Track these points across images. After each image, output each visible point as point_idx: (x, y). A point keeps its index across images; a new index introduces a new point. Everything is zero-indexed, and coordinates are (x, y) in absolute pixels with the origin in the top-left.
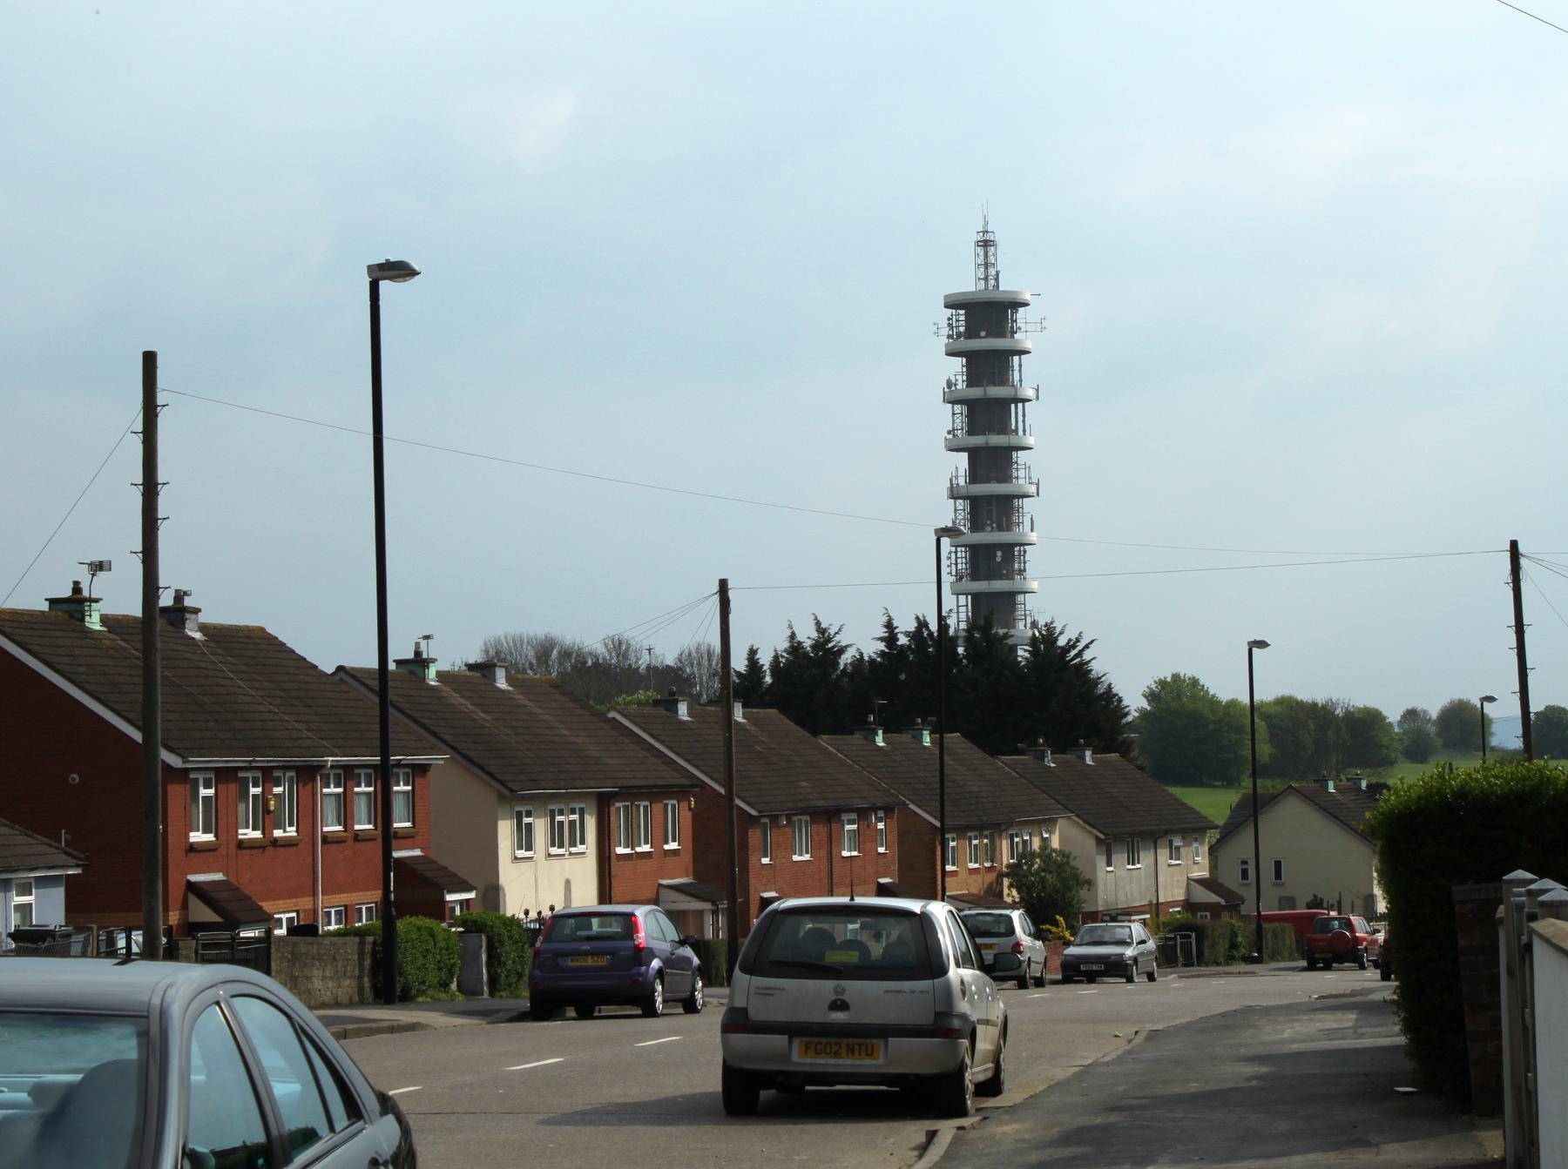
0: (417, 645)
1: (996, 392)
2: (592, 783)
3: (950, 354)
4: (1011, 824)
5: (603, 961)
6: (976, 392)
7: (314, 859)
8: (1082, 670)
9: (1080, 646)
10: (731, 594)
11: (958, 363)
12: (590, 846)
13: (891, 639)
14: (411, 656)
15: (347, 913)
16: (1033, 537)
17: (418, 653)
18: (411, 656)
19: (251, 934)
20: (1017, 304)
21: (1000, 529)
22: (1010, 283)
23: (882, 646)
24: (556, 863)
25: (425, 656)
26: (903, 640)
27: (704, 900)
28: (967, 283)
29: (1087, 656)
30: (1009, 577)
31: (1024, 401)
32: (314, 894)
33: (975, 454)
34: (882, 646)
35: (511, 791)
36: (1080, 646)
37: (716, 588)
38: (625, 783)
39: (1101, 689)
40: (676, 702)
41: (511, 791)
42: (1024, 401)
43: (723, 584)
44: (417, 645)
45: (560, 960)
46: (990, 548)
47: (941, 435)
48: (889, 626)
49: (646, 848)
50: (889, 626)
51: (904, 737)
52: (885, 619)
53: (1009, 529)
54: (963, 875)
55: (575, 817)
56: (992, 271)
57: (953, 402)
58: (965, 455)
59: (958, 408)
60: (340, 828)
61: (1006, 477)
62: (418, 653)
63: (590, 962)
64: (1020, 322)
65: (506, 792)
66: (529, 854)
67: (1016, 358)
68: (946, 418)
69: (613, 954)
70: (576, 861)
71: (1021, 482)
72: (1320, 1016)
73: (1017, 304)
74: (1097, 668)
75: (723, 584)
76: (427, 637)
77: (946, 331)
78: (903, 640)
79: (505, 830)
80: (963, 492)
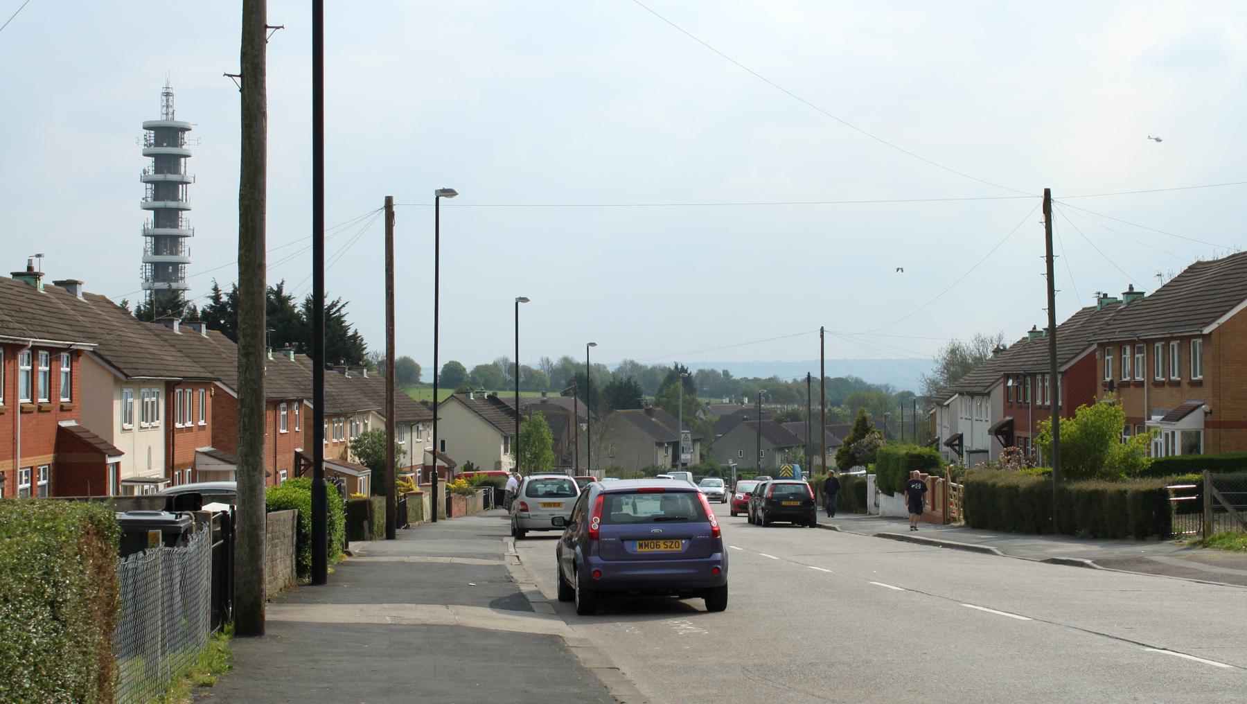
0: (30, 261)
1: (172, 177)
2: (143, 372)
3: (145, 155)
4: (354, 413)
5: (680, 546)
6: (160, 177)
7: (15, 426)
8: (339, 320)
9: (339, 305)
10: (395, 209)
11: (150, 161)
12: (160, 423)
13: (216, 298)
14: (25, 270)
15: (32, 473)
16: (190, 259)
17: (30, 268)
18: (25, 270)
19: (656, 530)
20: (185, 129)
21: (172, 254)
22: (180, 118)
23: (211, 302)
24: (143, 433)
25: (36, 270)
26: (224, 299)
27: (231, 463)
28: (157, 117)
29: (343, 312)
30: (176, 281)
31: (187, 183)
32: (14, 457)
33: (157, 211)
34: (211, 302)
35: (127, 376)
36: (339, 305)
37: (383, 204)
38: (183, 374)
39: (350, 333)
40: (172, 321)
41: (127, 376)
42: (187, 183)
43: (389, 202)
44: (30, 261)
45: (627, 545)
46: (165, 265)
47: (138, 200)
48: (216, 289)
49: (189, 424)
50: (216, 289)
51: (280, 355)
52: (213, 285)
53: (176, 254)
54: (330, 446)
55: (154, 399)
56: (171, 110)
57: (146, 182)
58: (152, 212)
59: (149, 186)
60: (28, 401)
61: (175, 225)
62: (30, 268)
63: (663, 547)
64: (186, 139)
65: (123, 377)
66: (130, 426)
67: (183, 160)
68: (143, 191)
69: (689, 538)
70: (150, 433)
71: (184, 227)
72: (488, 541)
73: (185, 129)
74: (348, 320)
75: (389, 202)
76: (39, 256)
77: (143, 142)
78: (224, 299)
79: (117, 406)
80: (151, 233)
